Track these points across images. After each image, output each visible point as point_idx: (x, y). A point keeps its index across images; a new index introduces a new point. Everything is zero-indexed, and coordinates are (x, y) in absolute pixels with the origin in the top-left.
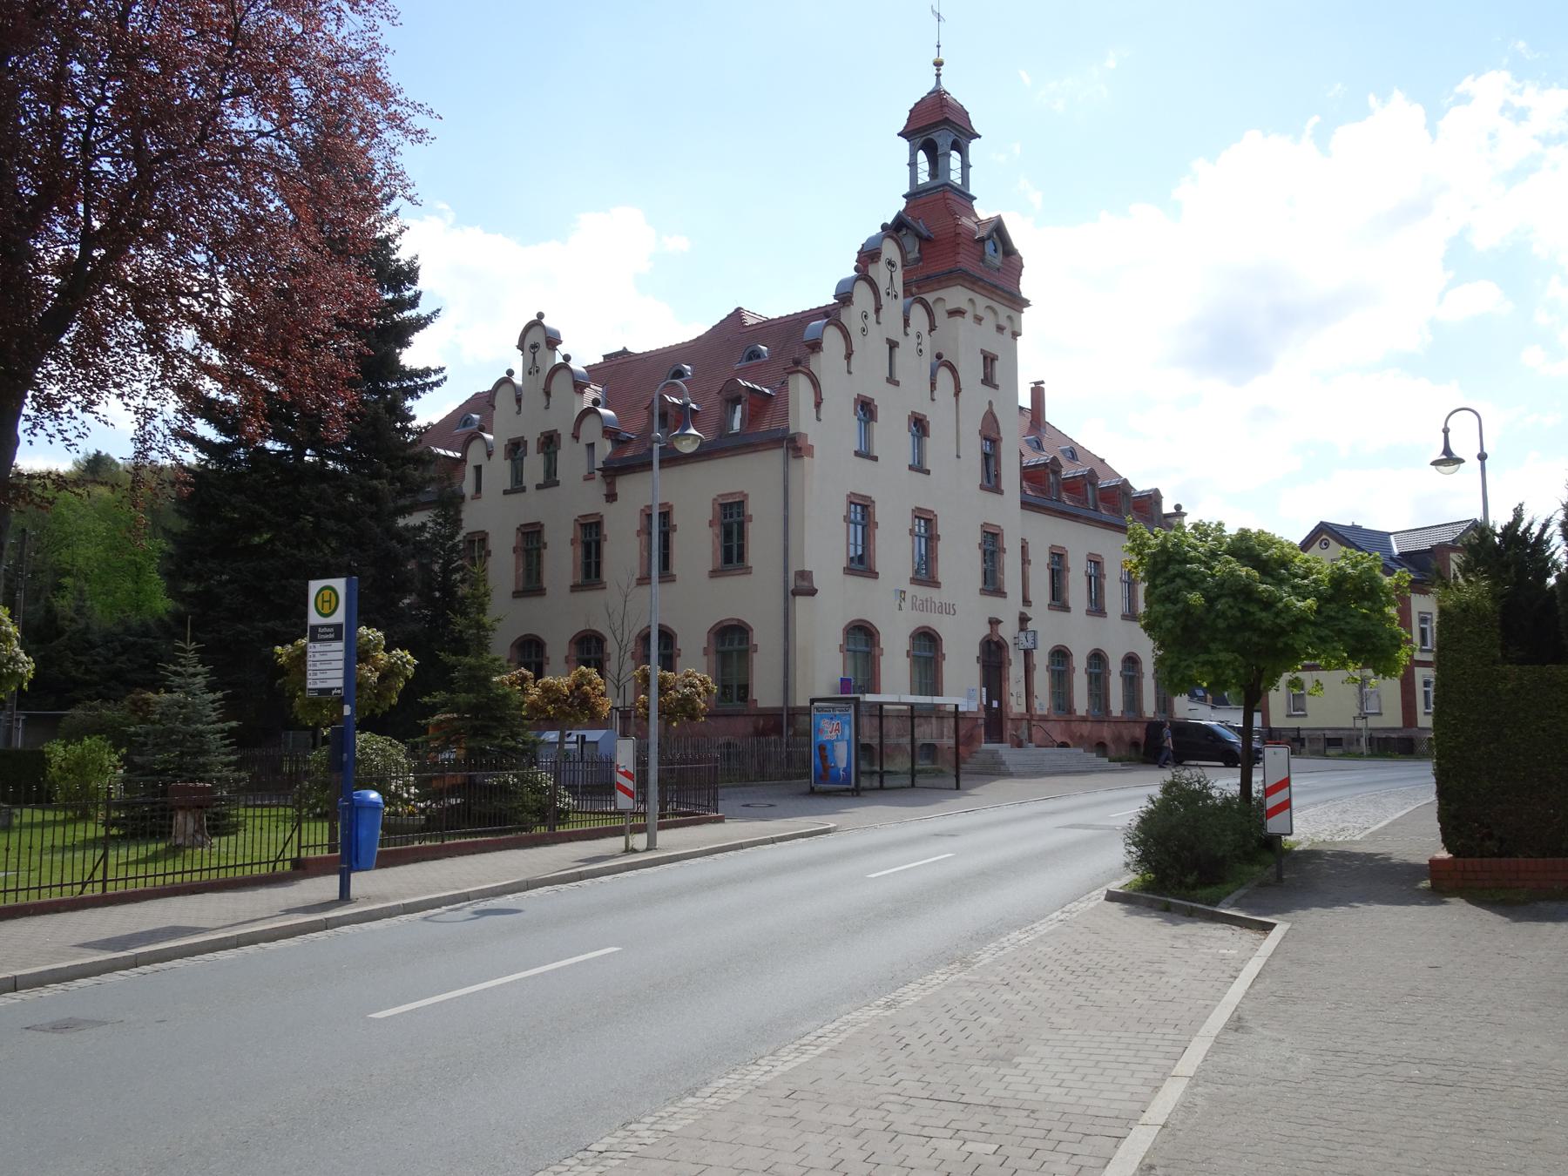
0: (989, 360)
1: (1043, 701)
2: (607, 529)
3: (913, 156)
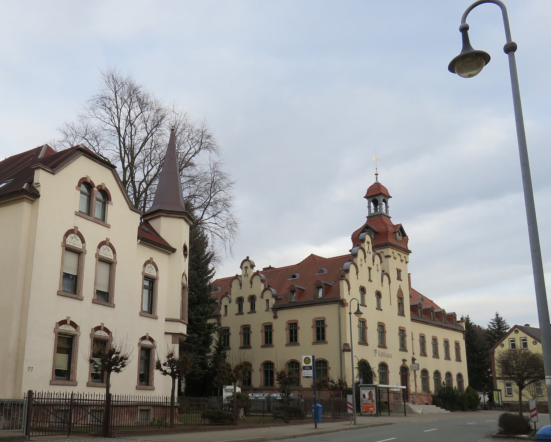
0: (399, 271)
1: (420, 389)
2: (274, 327)
3: (369, 204)
